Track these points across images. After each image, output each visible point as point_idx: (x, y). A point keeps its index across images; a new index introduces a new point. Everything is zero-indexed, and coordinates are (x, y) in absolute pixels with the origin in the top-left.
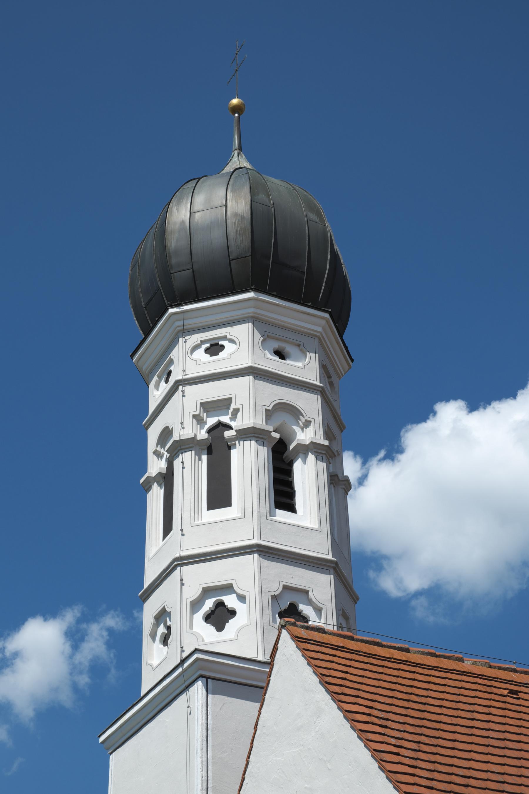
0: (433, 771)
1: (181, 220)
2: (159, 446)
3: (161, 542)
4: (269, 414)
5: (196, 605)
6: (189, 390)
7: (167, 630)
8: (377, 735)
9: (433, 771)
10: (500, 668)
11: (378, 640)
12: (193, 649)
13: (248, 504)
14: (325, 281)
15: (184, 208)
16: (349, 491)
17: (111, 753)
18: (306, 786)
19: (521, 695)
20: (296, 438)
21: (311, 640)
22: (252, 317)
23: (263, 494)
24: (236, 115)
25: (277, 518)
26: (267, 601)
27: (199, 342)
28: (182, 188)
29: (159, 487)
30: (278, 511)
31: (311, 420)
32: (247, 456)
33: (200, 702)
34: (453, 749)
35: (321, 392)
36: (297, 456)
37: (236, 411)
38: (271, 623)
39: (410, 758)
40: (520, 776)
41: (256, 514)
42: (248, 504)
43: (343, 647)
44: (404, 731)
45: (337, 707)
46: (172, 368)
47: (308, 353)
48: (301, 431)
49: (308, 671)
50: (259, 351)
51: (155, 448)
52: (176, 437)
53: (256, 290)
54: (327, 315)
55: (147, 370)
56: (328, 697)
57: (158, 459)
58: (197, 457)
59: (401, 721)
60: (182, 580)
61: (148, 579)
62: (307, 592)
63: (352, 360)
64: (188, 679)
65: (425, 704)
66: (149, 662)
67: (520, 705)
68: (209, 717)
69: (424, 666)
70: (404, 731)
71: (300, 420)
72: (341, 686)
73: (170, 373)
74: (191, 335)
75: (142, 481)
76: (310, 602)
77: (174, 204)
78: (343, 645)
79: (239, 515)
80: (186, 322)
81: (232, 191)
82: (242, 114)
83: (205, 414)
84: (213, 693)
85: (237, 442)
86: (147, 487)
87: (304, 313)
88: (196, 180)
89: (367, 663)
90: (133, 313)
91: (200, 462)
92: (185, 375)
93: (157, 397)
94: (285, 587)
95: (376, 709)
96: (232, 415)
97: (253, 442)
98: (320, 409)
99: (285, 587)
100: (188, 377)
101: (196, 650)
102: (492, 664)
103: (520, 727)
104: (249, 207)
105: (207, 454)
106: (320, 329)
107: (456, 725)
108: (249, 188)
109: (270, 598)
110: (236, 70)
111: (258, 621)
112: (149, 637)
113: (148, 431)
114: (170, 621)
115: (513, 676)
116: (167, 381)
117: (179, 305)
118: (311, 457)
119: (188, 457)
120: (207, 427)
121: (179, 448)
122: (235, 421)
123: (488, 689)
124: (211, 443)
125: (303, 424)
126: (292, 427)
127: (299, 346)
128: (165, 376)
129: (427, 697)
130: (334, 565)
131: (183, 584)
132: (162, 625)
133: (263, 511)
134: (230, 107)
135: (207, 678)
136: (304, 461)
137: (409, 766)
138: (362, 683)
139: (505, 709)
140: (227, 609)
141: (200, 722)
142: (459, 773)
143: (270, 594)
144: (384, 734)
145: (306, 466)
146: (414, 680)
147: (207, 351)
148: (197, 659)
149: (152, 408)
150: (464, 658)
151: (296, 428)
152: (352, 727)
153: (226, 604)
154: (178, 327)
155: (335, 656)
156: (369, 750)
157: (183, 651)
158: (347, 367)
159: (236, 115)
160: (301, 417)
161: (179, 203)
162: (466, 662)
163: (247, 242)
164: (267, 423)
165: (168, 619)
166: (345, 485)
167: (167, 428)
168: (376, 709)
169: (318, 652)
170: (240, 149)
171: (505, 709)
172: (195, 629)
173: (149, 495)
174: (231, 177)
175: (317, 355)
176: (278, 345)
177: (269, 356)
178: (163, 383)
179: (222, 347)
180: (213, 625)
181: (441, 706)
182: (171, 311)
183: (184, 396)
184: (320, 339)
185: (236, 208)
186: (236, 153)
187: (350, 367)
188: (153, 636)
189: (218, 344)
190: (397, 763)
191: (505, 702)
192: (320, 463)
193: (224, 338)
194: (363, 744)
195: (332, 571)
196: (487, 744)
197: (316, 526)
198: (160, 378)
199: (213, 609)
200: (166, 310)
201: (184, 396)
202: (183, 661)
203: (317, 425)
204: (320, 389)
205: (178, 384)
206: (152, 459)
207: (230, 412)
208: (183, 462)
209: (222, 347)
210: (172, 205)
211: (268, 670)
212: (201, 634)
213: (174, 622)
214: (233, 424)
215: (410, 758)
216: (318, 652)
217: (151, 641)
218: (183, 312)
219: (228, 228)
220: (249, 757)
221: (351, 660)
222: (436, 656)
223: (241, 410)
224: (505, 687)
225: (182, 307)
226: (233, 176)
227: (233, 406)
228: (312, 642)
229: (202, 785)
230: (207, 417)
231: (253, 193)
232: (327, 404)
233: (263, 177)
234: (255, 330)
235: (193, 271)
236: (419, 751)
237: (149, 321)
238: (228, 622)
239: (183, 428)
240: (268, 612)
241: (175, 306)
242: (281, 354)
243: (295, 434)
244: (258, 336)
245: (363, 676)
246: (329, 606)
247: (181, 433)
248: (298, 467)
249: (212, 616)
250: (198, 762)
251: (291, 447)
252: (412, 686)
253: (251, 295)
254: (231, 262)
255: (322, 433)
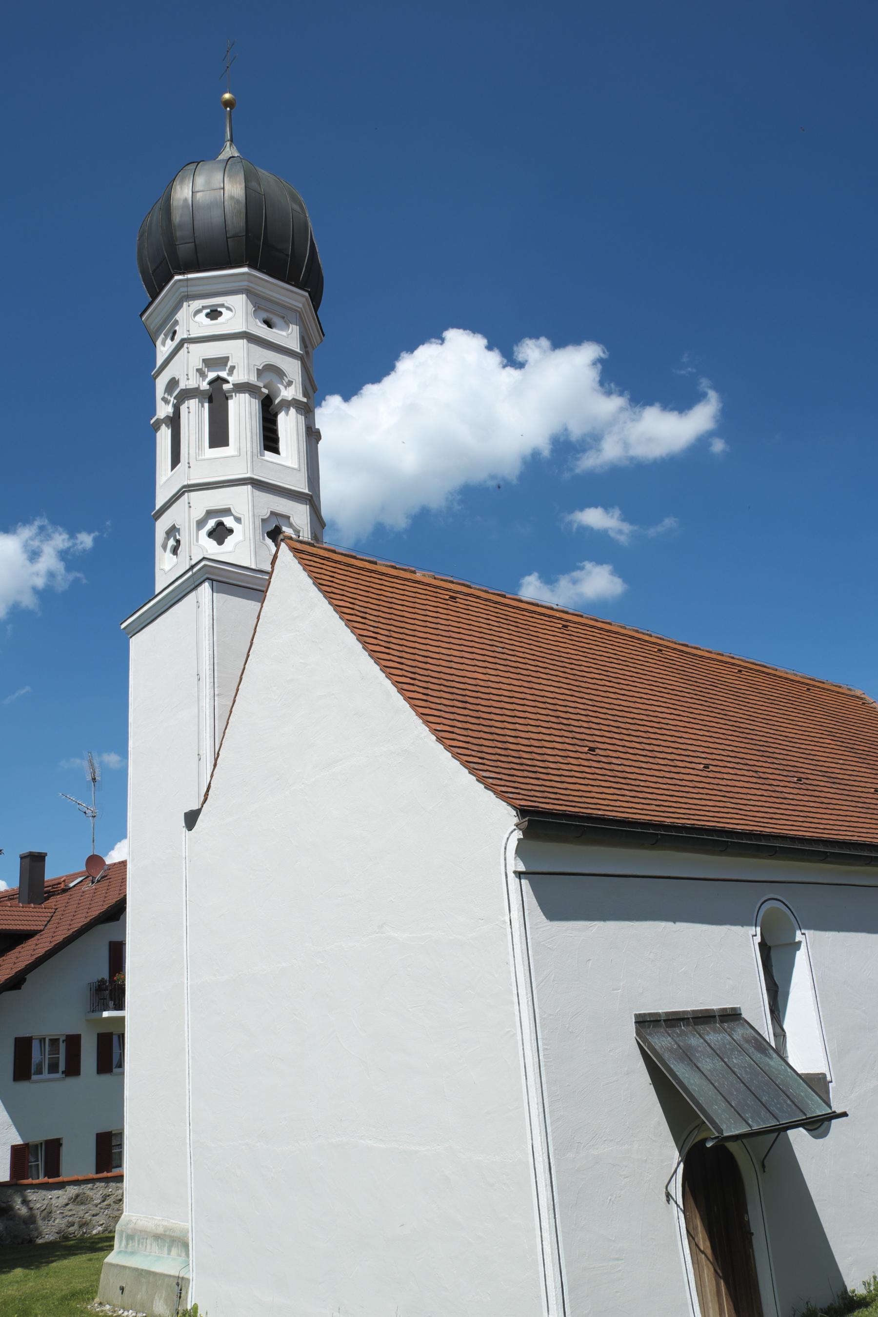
0: (402, 651)
1: (184, 197)
2: (166, 394)
3: (170, 473)
4: (260, 373)
5: (201, 524)
6: (193, 347)
7: (176, 543)
8: (360, 624)
9: (402, 651)
10: (442, 580)
11: (354, 554)
12: (201, 557)
13: (243, 446)
14: (305, 265)
15: (187, 187)
16: (319, 441)
17: (131, 637)
18: (301, 661)
19: (458, 600)
20: (280, 395)
21: (304, 551)
22: (246, 290)
23: (255, 437)
24: (228, 109)
25: (266, 458)
26: (259, 523)
27: (201, 307)
28: (184, 169)
29: (167, 428)
30: (266, 452)
31: (293, 380)
32: (242, 405)
33: (207, 600)
34: (414, 636)
35: (301, 358)
36: (281, 408)
37: (232, 368)
38: (261, 540)
39: (385, 641)
40: (462, 657)
41: (249, 453)
42: (243, 446)
43: (329, 558)
44: (379, 622)
45: (327, 602)
46: (177, 328)
47: (291, 325)
48: (284, 388)
49: (304, 575)
50: (251, 319)
51: (163, 396)
52: (182, 385)
53: (250, 266)
54: (307, 294)
55: (154, 328)
56: (320, 595)
57: (166, 404)
58: (200, 404)
59: (376, 614)
60: (189, 503)
61: (159, 503)
62: (288, 518)
63: (324, 335)
64: (197, 581)
65: (391, 603)
66: (162, 567)
67: (458, 607)
68: (214, 610)
69: (388, 576)
70: (379, 622)
71: (284, 380)
72: (330, 586)
73: (175, 332)
74: (194, 300)
75: (152, 422)
76: (291, 526)
77: (178, 182)
78: (329, 557)
79: (236, 453)
80: (189, 289)
81: (228, 176)
82: (233, 108)
83: (206, 369)
84: (218, 592)
85: (234, 394)
86: (156, 427)
87: (284, 288)
88: (197, 164)
89: (347, 571)
90: (141, 278)
91: (203, 409)
92: (189, 335)
93: (164, 352)
94: (272, 513)
95: (357, 605)
96: (229, 371)
97: (247, 395)
98: (300, 372)
99: (272, 513)
100: (192, 336)
101: (204, 559)
102: (436, 576)
103: (459, 622)
104: (243, 191)
105: (209, 403)
106: (301, 305)
107: (415, 619)
108: (243, 175)
109: (260, 520)
110: (228, 67)
111: (252, 538)
112: (161, 548)
113: (156, 380)
114: (179, 535)
115: (451, 586)
116: (172, 339)
117: (184, 273)
118: (292, 411)
119: (193, 403)
120: (208, 380)
121: (185, 396)
122: (231, 376)
123: (435, 595)
124: (211, 394)
125: (286, 383)
126: (278, 385)
127: (283, 318)
128: (171, 335)
129: (392, 598)
130: (309, 498)
131: (190, 507)
132: (172, 539)
133: (255, 451)
134: (223, 100)
135: (212, 580)
136: (287, 414)
137: (385, 647)
138: (345, 586)
139: (447, 609)
140: (226, 528)
141: (207, 614)
142: (420, 654)
143: (261, 517)
144: (365, 624)
145: (288, 418)
146: (382, 585)
147: (208, 315)
148: (205, 566)
149: (160, 361)
150: (417, 571)
151: (280, 386)
152: (340, 617)
153: (225, 524)
154: (183, 292)
155: (323, 564)
156: (355, 635)
157: (191, 559)
158: (319, 341)
159: (228, 109)
160: (285, 377)
161: (182, 182)
162: (417, 574)
163: (242, 223)
164: (258, 380)
165: (177, 534)
166: (317, 436)
167: (174, 378)
168: (357, 605)
169: (311, 560)
170: (231, 140)
171: (447, 609)
172: (200, 542)
173: (158, 434)
174: (227, 163)
175: (298, 327)
176: (267, 316)
177: (259, 324)
178: (169, 341)
179: (220, 313)
180: (215, 540)
181: (403, 605)
182: (177, 277)
183: (188, 352)
184: (300, 314)
185: (233, 192)
186: (228, 143)
187: (322, 340)
188: (164, 547)
189: (216, 310)
190: (376, 645)
191: (447, 605)
192: (300, 416)
193: (222, 306)
194: (350, 631)
195: (308, 502)
196: (438, 634)
197: (296, 466)
198: (166, 336)
199: (215, 527)
200: (172, 277)
201: (188, 352)
202: (192, 567)
203: (297, 385)
204: (300, 356)
205: (183, 342)
206: (160, 404)
207: (227, 368)
208: (188, 408)
209: (220, 313)
210: (176, 184)
211: (268, 578)
212: (206, 546)
213: (183, 537)
214: (230, 379)
215: (385, 641)
216: (311, 560)
217: (164, 552)
218: (187, 280)
219: (225, 210)
220: (252, 640)
221: (335, 568)
222: (396, 568)
223: (236, 367)
224: (446, 594)
225: (186, 275)
226: (228, 163)
227: (230, 364)
228: (305, 553)
229: (210, 661)
230: (208, 371)
231: (247, 180)
232: (305, 368)
233: (255, 168)
234: (248, 300)
235: (195, 244)
236: (390, 636)
237: (156, 286)
238: (227, 538)
239: (188, 379)
240: (259, 531)
241: (180, 274)
242: (268, 324)
243: (280, 391)
244: (251, 306)
245: (345, 581)
246: (306, 529)
247: (187, 383)
248: (281, 418)
249: (214, 533)
250: (206, 644)
251: (277, 401)
252: (381, 590)
253: (245, 270)
254: (228, 239)
255: (301, 391)
